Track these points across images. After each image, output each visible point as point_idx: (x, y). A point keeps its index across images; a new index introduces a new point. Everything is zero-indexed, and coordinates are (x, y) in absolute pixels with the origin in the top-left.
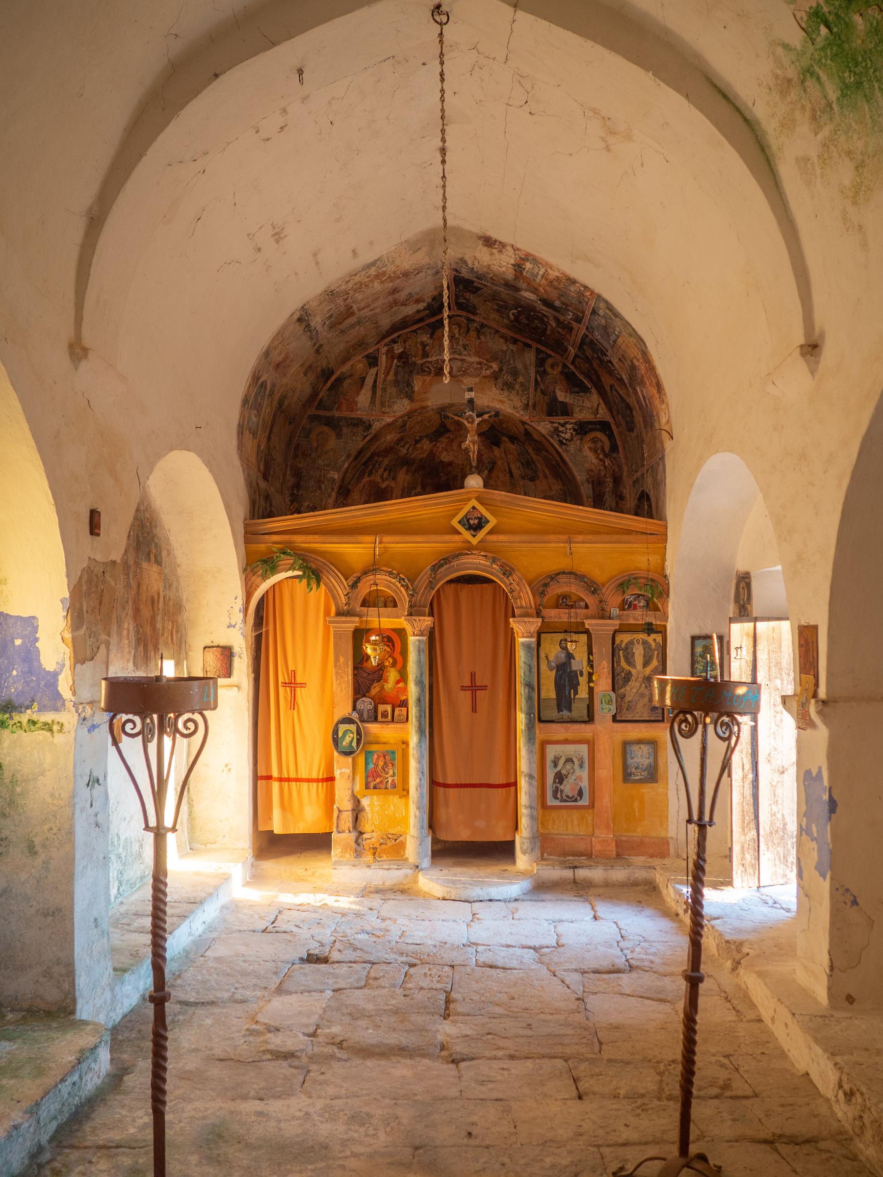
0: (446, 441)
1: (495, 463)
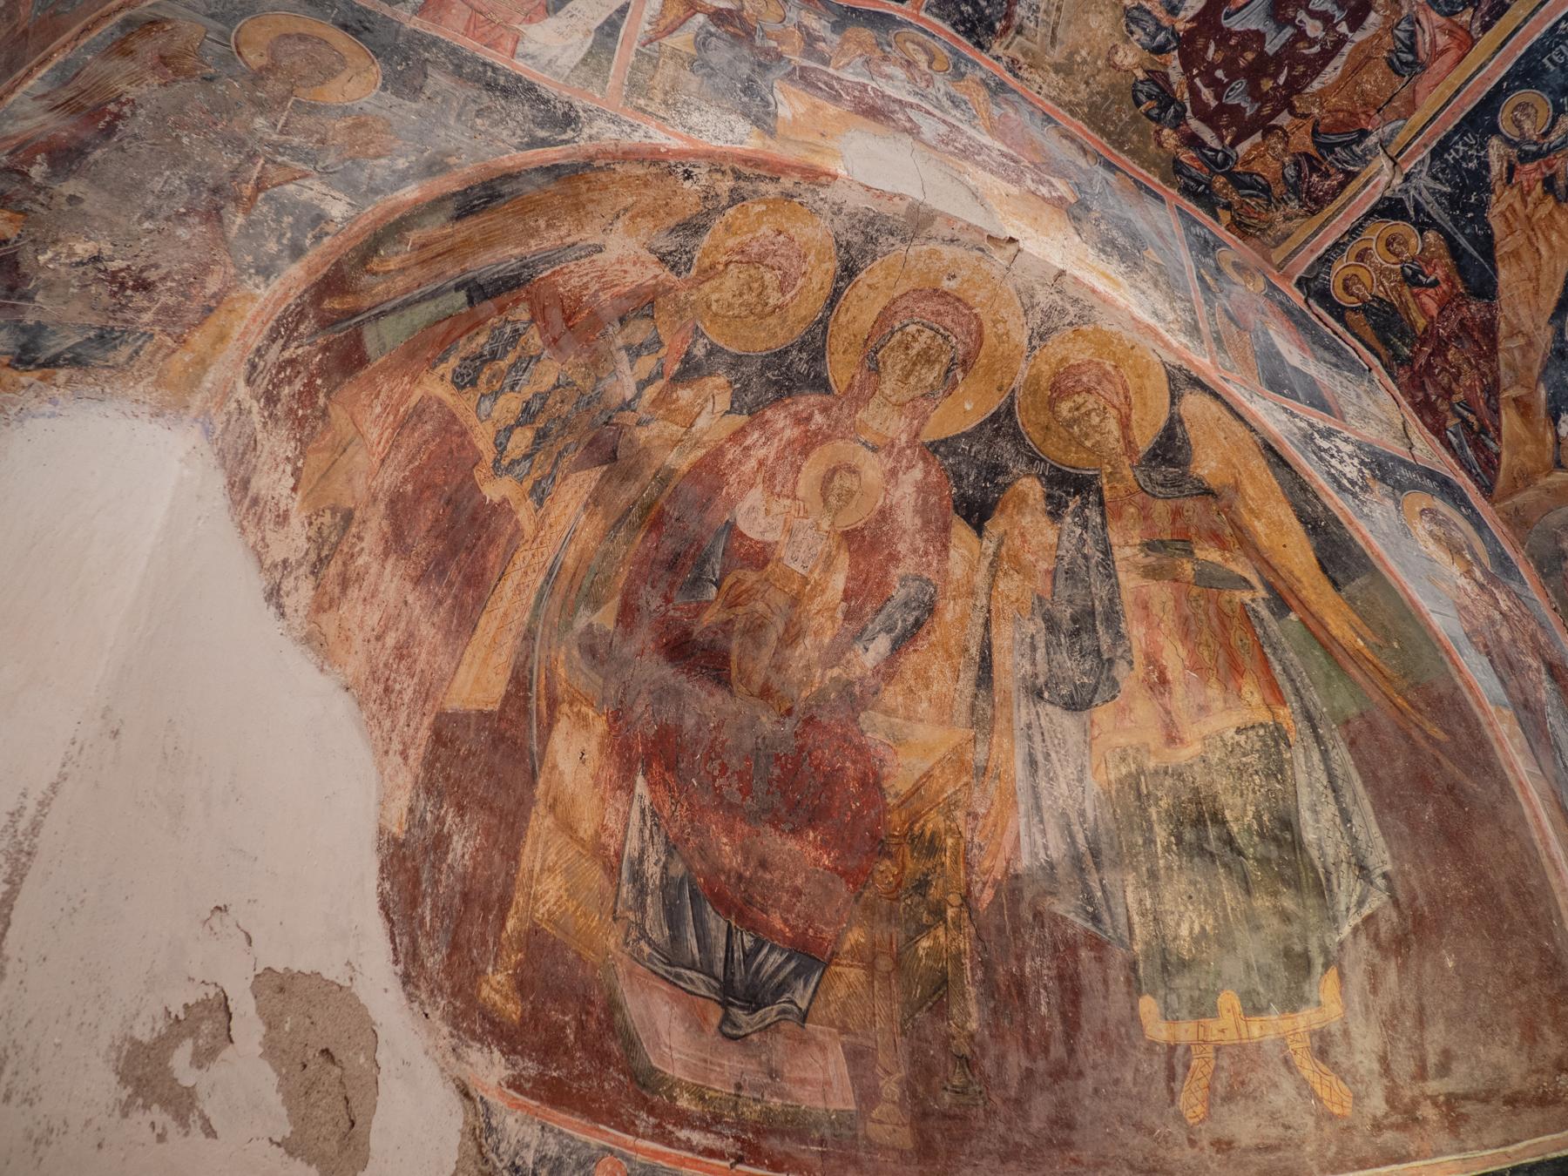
0: (791, 433)
1: (931, 609)
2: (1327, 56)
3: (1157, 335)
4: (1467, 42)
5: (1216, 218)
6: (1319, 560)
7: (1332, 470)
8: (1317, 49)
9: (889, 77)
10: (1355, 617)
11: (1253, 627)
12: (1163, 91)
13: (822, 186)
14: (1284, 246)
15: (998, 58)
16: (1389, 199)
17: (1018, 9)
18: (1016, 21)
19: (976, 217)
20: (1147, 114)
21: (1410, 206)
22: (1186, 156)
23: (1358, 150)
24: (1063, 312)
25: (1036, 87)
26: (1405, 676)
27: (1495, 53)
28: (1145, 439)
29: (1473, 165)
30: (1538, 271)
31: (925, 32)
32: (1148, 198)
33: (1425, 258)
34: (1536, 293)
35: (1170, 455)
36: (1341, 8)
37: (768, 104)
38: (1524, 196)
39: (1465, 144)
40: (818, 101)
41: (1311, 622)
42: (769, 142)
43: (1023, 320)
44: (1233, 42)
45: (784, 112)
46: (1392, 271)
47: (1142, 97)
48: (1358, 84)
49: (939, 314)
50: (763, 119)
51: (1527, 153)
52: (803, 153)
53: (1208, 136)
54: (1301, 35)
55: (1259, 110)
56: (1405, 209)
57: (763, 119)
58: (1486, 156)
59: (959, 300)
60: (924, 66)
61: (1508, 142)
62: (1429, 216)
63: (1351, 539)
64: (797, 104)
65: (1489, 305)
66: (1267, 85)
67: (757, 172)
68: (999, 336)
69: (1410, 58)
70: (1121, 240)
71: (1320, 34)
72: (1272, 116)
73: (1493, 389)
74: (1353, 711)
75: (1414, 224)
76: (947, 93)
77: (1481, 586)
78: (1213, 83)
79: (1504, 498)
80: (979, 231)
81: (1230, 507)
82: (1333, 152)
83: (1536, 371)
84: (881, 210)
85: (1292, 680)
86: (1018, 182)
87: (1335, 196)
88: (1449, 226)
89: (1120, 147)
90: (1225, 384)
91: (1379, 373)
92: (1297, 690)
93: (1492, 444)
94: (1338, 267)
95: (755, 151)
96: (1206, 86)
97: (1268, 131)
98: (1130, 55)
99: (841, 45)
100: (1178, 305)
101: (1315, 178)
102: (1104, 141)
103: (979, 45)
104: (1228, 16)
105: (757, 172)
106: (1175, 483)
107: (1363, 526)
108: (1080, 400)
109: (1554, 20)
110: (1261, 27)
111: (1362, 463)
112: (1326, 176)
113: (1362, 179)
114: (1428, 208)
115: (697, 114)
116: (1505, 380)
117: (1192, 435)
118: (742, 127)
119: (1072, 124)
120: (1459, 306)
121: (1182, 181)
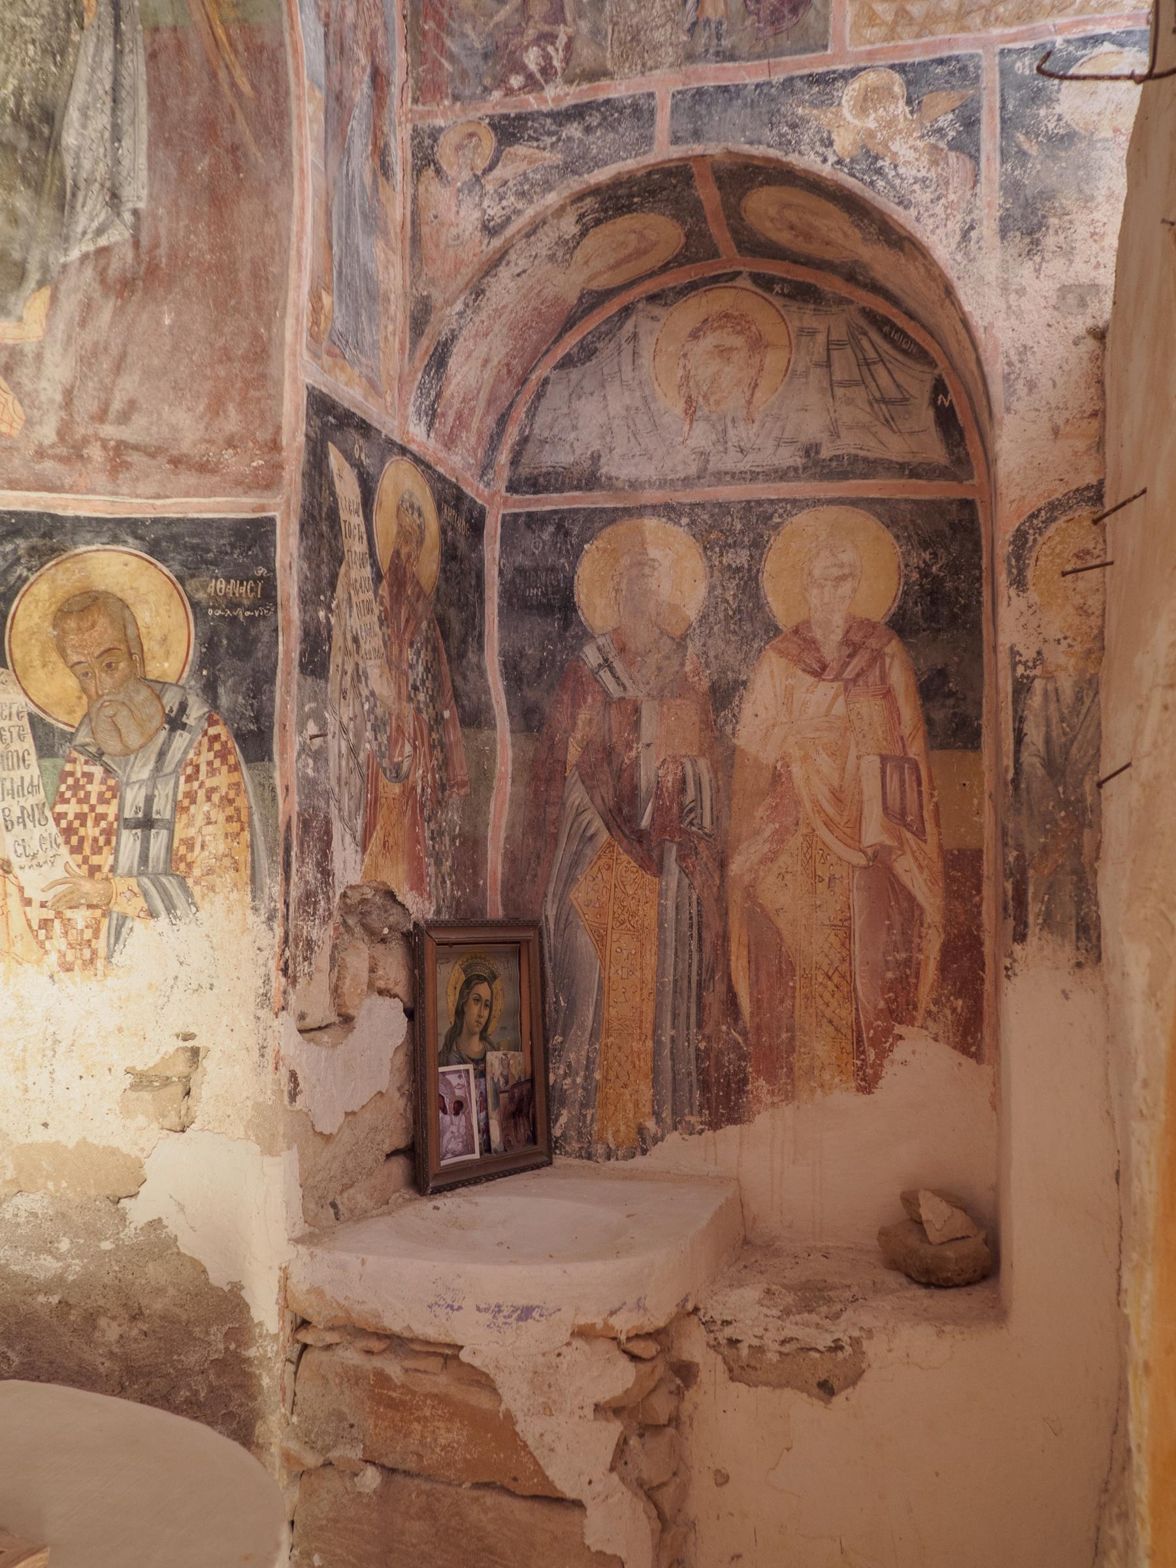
74: (167, 20)
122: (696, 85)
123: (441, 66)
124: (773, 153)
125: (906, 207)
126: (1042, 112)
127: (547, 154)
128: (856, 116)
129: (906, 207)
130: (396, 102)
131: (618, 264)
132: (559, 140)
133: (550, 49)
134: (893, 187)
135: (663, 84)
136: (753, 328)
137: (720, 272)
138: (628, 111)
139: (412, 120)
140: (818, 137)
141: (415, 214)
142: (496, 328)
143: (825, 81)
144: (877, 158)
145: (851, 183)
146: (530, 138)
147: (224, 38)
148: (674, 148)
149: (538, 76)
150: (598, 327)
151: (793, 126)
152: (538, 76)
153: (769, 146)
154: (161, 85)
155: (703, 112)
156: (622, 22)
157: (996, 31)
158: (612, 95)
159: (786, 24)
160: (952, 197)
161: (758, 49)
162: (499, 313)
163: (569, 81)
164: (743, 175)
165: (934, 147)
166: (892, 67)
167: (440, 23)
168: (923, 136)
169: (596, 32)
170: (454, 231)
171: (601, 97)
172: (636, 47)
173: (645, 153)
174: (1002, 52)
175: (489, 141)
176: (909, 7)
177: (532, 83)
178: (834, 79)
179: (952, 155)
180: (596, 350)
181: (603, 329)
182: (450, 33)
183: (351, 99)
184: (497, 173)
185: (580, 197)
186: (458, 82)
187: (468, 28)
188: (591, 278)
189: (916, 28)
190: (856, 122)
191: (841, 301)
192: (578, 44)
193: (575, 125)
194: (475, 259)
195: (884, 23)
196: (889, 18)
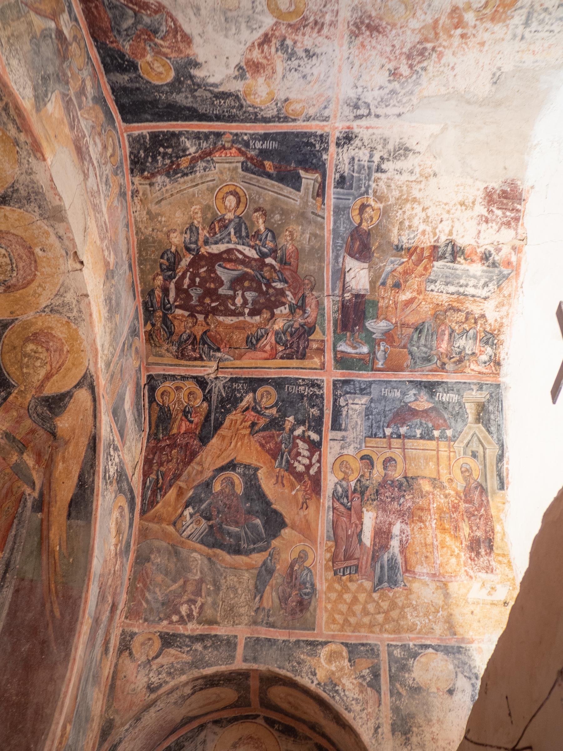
2: (233, 313)
3: (96, 355)
4: (273, 357)
5: (145, 324)
6: (72, 500)
7: (107, 466)
8: (233, 308)
9: (95, 143)
10: (65, 535)
11: (19, 506)
12: (174, 263)
13: (35, 156)
14: (157, 358)
15: (133, 183)
16: (205, 379)
17: (159, 177)
18: (154, 180)
19: (78, 239)
20: (161, 265)
21: (208, 388)
22: (158, 293)
23: (212, 353)
24: (71, 310)
25: (135, 210)
26: (64, 576)
27: (277, 368)
28: (50, 390)
29: (238, 395)
30: (225, 450)
31: (119, 142)
32: (132, 293)
33: (196, 410)
34: (218, 457)
35: (53, 406)
36: (252, 304)
37: (46, 96)
38: (243, 421)
39: (242, 386)
40: (65, 120)
41: (45, 523)
42: (34, 112)
43: (52, 297)
44: (212, 275)
45: (50, 107)
46: (182, 404)
47: (166, 257)
48: (233, 332)
49: (21, 258)
50: (40, 100)
51: (256, 408)
52: (42, 134)
53: (172, 294)
54: (233, 298)
55: (196, 306)
56: (206, 387)
57: (40, 100)
58: (245, 397)
59: (36, 261)
60: (109, 154)
61: (255, 399)
62: (211, 398)
63: (92, 502)
64: (57, 111)
65: (201, 446)
66: (207, 301)
67: (16, 118)
68: (35, 292)
69: (255, 342)
70: (113, 302)
71: (239, 305)
72: (198, 312)
73: (177, 477)
74: (29, 576)
75: (204, 396)
76: (107, 175)
77: (116, 554)
78: (192, 280)
79: (146, 520)
80: (75, 245)
81: (57, 448)
82: (204, 345)
83: (195, 483)
84: (47, 194)
85: (15, 543)
86: (102, 240)
87: (190, 360)
88: (213, 407)
89: (140, 264)
90: (101, 397)
91: (145, 435)
92: (13, 548)
93: (159, 496)
94: (167, 384)
95: (25, 110)
96: (189, 279)
97: (192, 315)
98: (178, 239)
99: (91, 108)
100: (111, 349)
101: (190, 347)
102: (137, 255)
103: (132, 171)
104: (220, 266)
105: (16, 118)
106: (44, 419)
107: (100, 498)
108: (40, 350)
109: (300, 377)
110: (225, 281)
111: (117, 470)
112: (194, 350)
113: (203, 364)
114: (213, 395)
115: (17, 61)
116: (183, 478)
117: (70, 406)
118: (29, 92)
119: (133, 236)
120: (191, 437)
121: (147, 299)
122: (256, 636)
123: (141, 604)
124: (289, 674)
125: (349, 712)
126: (407, 675)
127: (184, 655)
128: (326, 663)
129: (349, 712)
130: (118, 617)
131: (204, 706)
132: (191, 650)
133: (193, 607)
134: (343, 700)
135: (242, 633)
136: (263, 746)
137: (250, 713)
138: (225, 642)
139: (123, 626)
140: (309, 670)
141: (115, 673)
142: (140, 736)
143: (314, 645)
144: (336, 685)
145: (324, 695)
146: (178, 646)
147: (54, 589)
148: (244, 664)
149: (186, 618)
150: (186, 734)
151: (299, 663)
152: (186, 618)
153: (288, 671)
154: (17, 605)
155: (259, 649)
156: (226, 601)
157: (385, 636)
158: (219, 633)
159: (297, 616)
160: (370, 710)
161: (285, 625)
162: (144, 728)
163: (199, 623)
164: (273, 680)
165: (361, 684)
166: (342, 643)
167: (145, 585)
168: (356, 678)
169: (214, 603)
170: (133, 686)
171: (213, 633)
172: (231, 613)
173: (231, 664)
174: (388, 645)
175: (157, 644)
176: (349, 619)
177: (182, 621)
178: (317, 645)
179: (369, 689)
180: (184, 746)
181: (189, 735)
182: (149, 590)
183: (101, 620)
184: (159, 660)
185: (197, 679)
186: (148, 613)
187: (157, 590)
188: (189, 712)
189: (352, 629)
190: (327, 666)
191: (307, 738)
192: (206, 607)
193: (200, 644)
194: (141, 703)
195: (338, 623)
196: (341, 622)
